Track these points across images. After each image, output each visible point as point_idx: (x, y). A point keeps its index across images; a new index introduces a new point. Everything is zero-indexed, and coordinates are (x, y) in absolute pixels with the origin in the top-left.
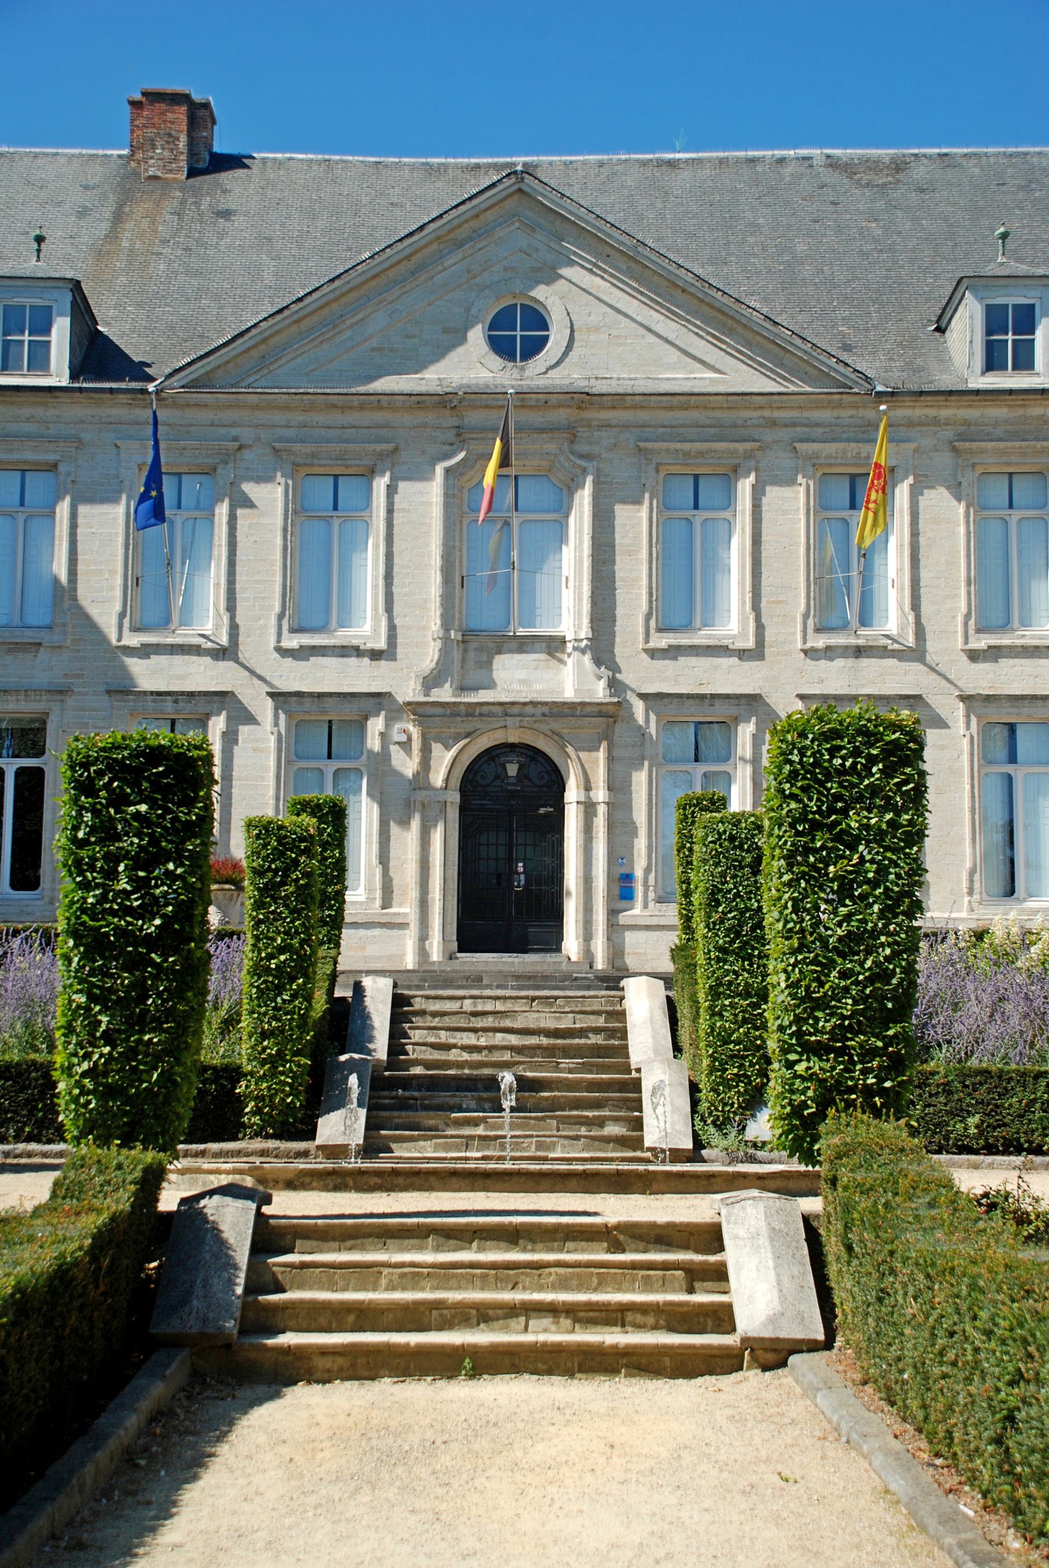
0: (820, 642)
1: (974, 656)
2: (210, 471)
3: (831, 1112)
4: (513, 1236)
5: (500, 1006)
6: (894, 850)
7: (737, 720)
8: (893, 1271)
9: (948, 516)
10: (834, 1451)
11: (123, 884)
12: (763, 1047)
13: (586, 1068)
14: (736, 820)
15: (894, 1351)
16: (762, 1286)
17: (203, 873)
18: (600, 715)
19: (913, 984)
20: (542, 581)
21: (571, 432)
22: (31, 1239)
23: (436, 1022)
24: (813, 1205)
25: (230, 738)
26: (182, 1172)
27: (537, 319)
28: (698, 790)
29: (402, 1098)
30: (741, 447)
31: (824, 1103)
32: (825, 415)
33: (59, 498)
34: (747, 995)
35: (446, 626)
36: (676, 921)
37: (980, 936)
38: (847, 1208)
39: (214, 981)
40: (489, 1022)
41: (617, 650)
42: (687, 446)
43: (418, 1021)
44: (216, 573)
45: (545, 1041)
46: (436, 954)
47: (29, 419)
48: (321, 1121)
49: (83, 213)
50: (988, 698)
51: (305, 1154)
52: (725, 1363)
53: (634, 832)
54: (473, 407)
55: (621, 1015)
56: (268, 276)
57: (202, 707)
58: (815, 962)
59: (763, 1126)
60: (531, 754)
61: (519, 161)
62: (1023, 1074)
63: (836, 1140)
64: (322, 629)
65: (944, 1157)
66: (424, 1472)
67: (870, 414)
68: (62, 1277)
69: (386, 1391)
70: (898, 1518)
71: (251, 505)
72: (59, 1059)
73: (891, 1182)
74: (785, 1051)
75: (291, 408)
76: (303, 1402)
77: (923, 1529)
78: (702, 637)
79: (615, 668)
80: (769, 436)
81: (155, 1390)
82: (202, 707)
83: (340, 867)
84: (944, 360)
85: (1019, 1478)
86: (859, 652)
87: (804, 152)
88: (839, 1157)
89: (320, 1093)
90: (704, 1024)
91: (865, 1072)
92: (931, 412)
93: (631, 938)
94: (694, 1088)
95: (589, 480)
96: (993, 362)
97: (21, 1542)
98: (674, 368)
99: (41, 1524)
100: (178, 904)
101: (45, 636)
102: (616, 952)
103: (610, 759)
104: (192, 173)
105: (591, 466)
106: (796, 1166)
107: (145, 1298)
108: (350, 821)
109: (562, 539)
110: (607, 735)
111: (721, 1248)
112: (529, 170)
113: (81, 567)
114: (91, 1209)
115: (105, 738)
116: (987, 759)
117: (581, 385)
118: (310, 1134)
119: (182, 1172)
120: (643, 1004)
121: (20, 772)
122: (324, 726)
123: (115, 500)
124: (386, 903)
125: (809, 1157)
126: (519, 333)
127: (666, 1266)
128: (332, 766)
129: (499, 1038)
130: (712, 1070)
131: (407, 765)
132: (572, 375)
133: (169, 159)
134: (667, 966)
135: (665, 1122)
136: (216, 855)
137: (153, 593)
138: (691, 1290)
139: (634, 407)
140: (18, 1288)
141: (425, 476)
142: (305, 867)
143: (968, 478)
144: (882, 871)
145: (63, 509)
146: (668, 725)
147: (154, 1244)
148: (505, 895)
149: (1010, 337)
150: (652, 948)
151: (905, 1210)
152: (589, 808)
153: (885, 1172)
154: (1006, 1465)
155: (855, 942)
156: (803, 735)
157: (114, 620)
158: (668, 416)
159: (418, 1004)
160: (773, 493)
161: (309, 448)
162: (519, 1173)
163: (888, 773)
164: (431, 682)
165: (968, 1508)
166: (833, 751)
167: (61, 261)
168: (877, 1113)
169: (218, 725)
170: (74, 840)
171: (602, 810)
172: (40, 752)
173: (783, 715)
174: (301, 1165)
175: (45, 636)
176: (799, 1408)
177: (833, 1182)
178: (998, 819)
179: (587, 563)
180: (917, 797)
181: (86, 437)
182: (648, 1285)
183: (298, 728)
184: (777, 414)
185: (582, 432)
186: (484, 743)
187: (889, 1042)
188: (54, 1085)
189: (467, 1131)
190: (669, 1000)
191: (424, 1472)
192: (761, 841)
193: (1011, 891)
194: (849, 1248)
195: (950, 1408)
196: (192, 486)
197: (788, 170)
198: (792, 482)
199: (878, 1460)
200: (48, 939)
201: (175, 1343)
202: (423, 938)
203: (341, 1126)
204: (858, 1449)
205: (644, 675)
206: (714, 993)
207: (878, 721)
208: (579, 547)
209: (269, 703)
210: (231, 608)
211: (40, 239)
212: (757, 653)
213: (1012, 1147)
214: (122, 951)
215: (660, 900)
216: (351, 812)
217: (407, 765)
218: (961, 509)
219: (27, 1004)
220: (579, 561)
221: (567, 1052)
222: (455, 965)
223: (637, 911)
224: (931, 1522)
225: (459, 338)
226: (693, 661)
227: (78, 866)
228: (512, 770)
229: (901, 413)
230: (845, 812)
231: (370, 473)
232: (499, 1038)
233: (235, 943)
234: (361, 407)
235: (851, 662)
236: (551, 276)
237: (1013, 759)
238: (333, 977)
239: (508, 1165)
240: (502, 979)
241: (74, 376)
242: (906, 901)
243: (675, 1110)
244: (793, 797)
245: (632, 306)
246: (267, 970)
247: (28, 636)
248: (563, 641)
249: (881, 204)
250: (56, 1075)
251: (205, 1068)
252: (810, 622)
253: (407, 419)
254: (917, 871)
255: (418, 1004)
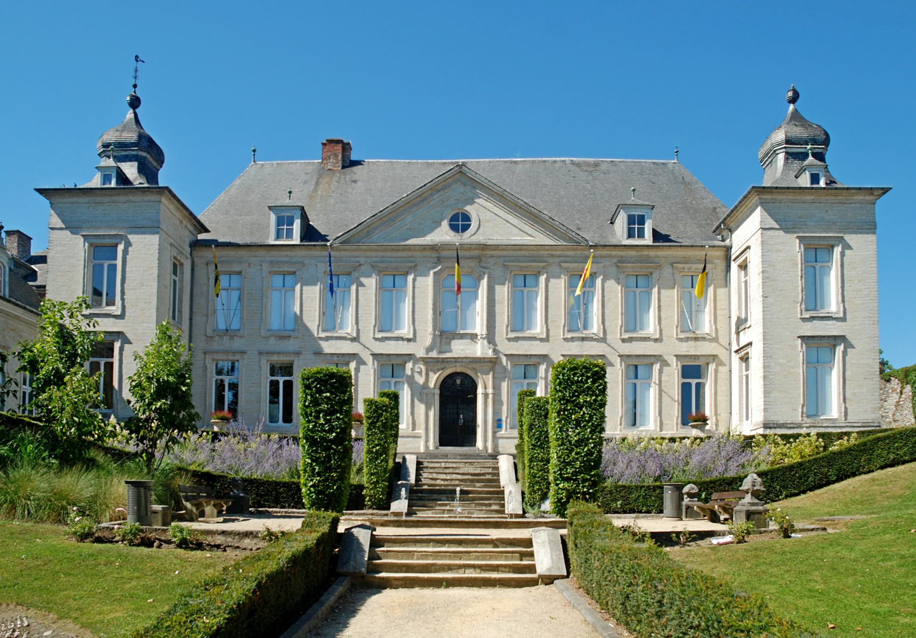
0: (569, 335)
1: (623, 341)
2: (349, 274)
3: (571, 500)
4: (460, 542)
5: (454, 465)
6: (596, 410)
7: (539, 364)
8: (591, 553)
9: (615, 290)
10: (568, 609)
11: (322, 421)
12: (548, 479)
13: (484, 486)
14: (539, 400)
15: (590, 578)
16: (546, 557)
17: (350, 418)
18: (490, 362)
19: (601, 457)
20: (469, 313)
21: (479, 259)
22: (296, 540)
23: (432, 470)
24: (564, 531)
25: (357, 370)
26: (345, 520)
27: (467, 218)
28: (525, 389)
29: (421, 496)
30: (541, 264)
31: (569, 497)
32: (571, 253)
33: (296, 284)
34: (542, 461)
35: (434, 330)
36: (518, 436)
37: (624, 440)
38: (576, 532)
39: (354, 455)
40: (451, 470)
41: (496, 338)
42: (521, 264)
43: (425, 470)
44: (351, 310)
45: (470, 477)
46: (431, 448)
47: (286, 256)
48: (392, 504)
49: (305, 183)
50: (628, 356)
51: (387, 515)
52: (533, 583)
53: (502, 404)
54: (444, 250)
55: (497, 468)
56: (370, 203)
57: (347, 359)
58: (567, 449)
59: (547, 506)
60: (465, 376)
61: (460, 161)
62: (637, 487)
63: (573, 510)
64: (390, 330)
65: (609, 515)
66: (431, 617)
67: (588, 253)
68: (307, 552)
69: (417, 591)
70: (590, 628)
71: (364, 286)
72: (302, 481)
73: (592, 523)
74: (555, 480)
75: (378, 251)
76: (388, 595)
77: (597, 631)
78: (527, 334)
79: (495, 345)
80: (551, 260)
81: (339, 589)
82: (347, 359)
83: (397, 416)
84: (613, 234)
85: (629, 615)
86: (583, 339)
87: (563, 159)
88: (574, 515)
89: (391, 494)
90: (527, 471)
91: (583, 487)
92: (609, 253)
93: (501, 442)
94: (523, 493)
95: (486, 276)
96: (630, 235)
97: (300, 632)
98: (517, 236)
99: (306, 627)
100: (341, 429)
101: (292, 334)
102: (496, 447)
103: (494, 378)
104: (343, 167)
105: (487, 271)
106: (558, 519)
107: (335, 560)
108: (400, 400)
109: (476, 298)
110: (492, 369)
111: (532, 546)
112: (464, 164)
113: (304, 309)
114: (315, 531)
115: (315, 370)
116: (627, 378)
117: (483, 242)
118: (388, 508)
119: (345, 520)
120: (505, 465)
121: (285, 382)
122: (391, 366)
123: (316, 284)
124: (414, 429)
125: (563, 516)
126: (460, 223)
127: (513, 552)
128: (394, 380)
129: (454, 476)
130: (529, 487)
131: (421, 380)
132: (480, 238)
133: (335, 163)
134: (514, 451)
135: (513, 505)
136: (354, 412)
137: (329, 318)
138: (521, 560)
139: (502, 250)
140: (293, 555)
141: (427, 275)
142: (385, 415)
143: (622, 276)
144: (591, 417)
145: (298, 288)
146: (514, 365)
147: (335, 546)
148: (456, 426)
149: (636, 226)
150: (509, 445)
151: (596, 532)
152: (486, 395)
153: (589, 520)
154: (625, 611)
155: (581, 442)
156: (564, 369)
157: (316, 328)
158: (515, 253)
159: (425, 464)
160: (553, 281)
161: (384, 265)
162: (462, 522)
163: (594, 382)
164: (429, 349)
165: (612, 624)
166: (574, 375)
167: (296, 201)
168: (587, 501)
169: (353, 365)
170: (304, 405)
171: (491, 396)
172: (291, 375)
173: (556, 362)
174: (386, 518)
175: (292, 334)
176: (557, 597)
177: (571, 524)
178: (631, 399)
179: (485, 307)
180: (603, 392)
181: (306, 262)
182: (506, 559)
183: (382, 366)
184: (554, 253)
185: (484, 259)
186: (448, 372)
187: (592, 476)
188: (301, 490)
189: (443, 508)
190: (515, 464)
191: (431, 617)
192: (549, 407)
193: (634, 424)
194: (576, 546)
195: (608, 595)
196: (343, 279)
197: (557, 165)
198: (559, 277)
199: (583, 611)
200: (296, 439)
201: (345, 575)
202: (427, 441)
203: (400, 505)
204: (576, 608)
205: (506, 347)
206: (531, 461)
207: (591, 364)
208: (482, 301)
209: (371, 357)
210: (357, 323)
211: (290, 192)
212: (546, 340)
213: (632, 511)
214: (322, 445)
215: (511, 428)
216: (400, 396)
217: (421, 380)
218: (620, 288)
219: (289, 462)
220: (482, 306)
221: (478, 481)
222: (436, 451)
223: (503, 432)
224: (600, 629)
225: (438, 224)
226: (524, 342)
227: (306, 415)
228: (458, 382)
229: (599, 253)
230: (578, 396)
231: (406, 274)
232: (454, 476)
233: (360, 442)
234: (403, 250)
235: (580, 343)
236: (471, 202)
237: (636, 377)
238: (395, 455)
239: (458, 519)
240: (455, 456)
241: (302, 240)
242: (599, 428)
243: (516, 501)
244: (560, 391)
245: (502, 213)
246: (372, 452)
247: (286, 334)
248: (476, 335)
249: (590, 178)
250: (302, 486)
251: (352, 485)
252: (566, 328)
253: (420, 254)
254: (603, 417)
255: (425, 464)
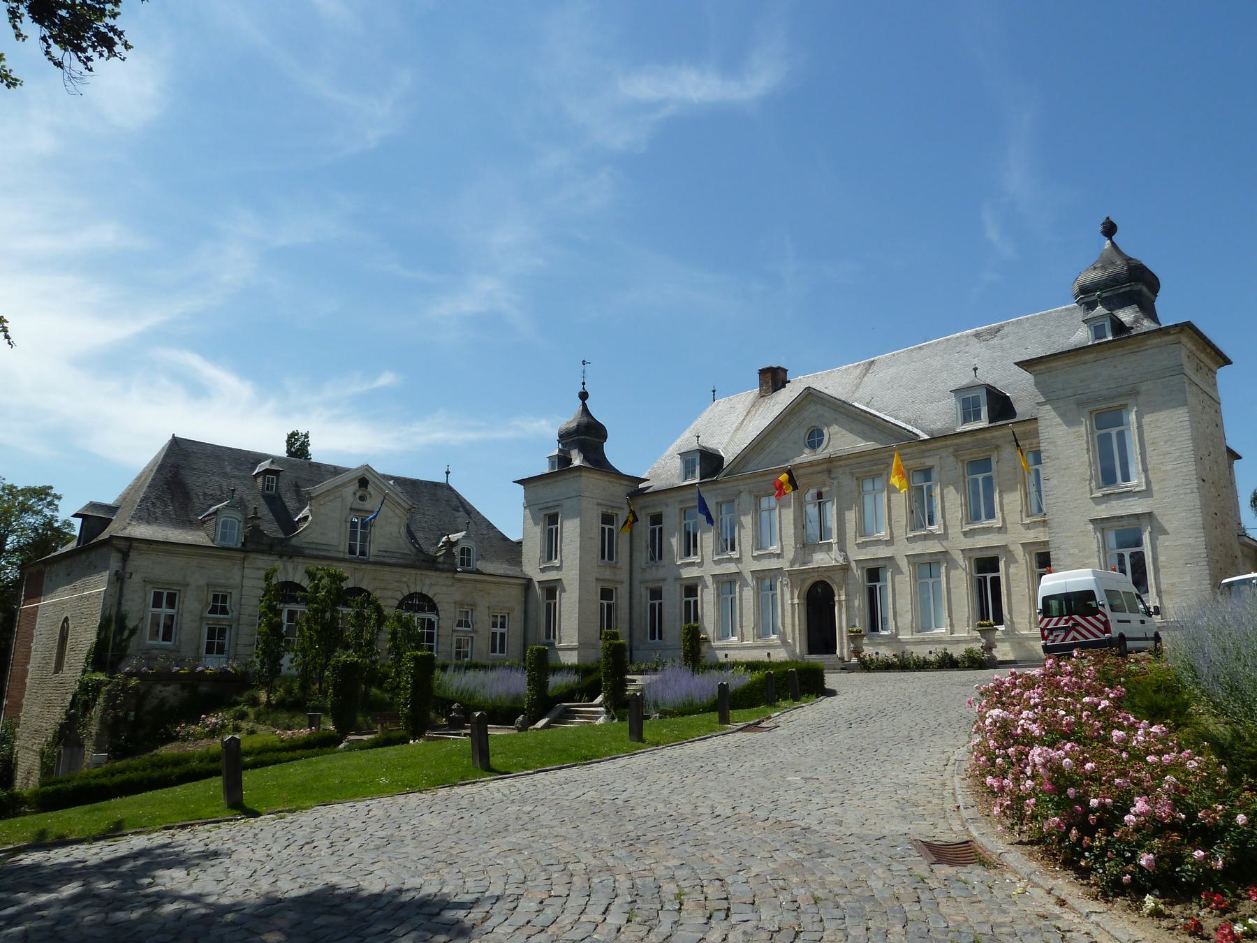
164: (792, 563)
